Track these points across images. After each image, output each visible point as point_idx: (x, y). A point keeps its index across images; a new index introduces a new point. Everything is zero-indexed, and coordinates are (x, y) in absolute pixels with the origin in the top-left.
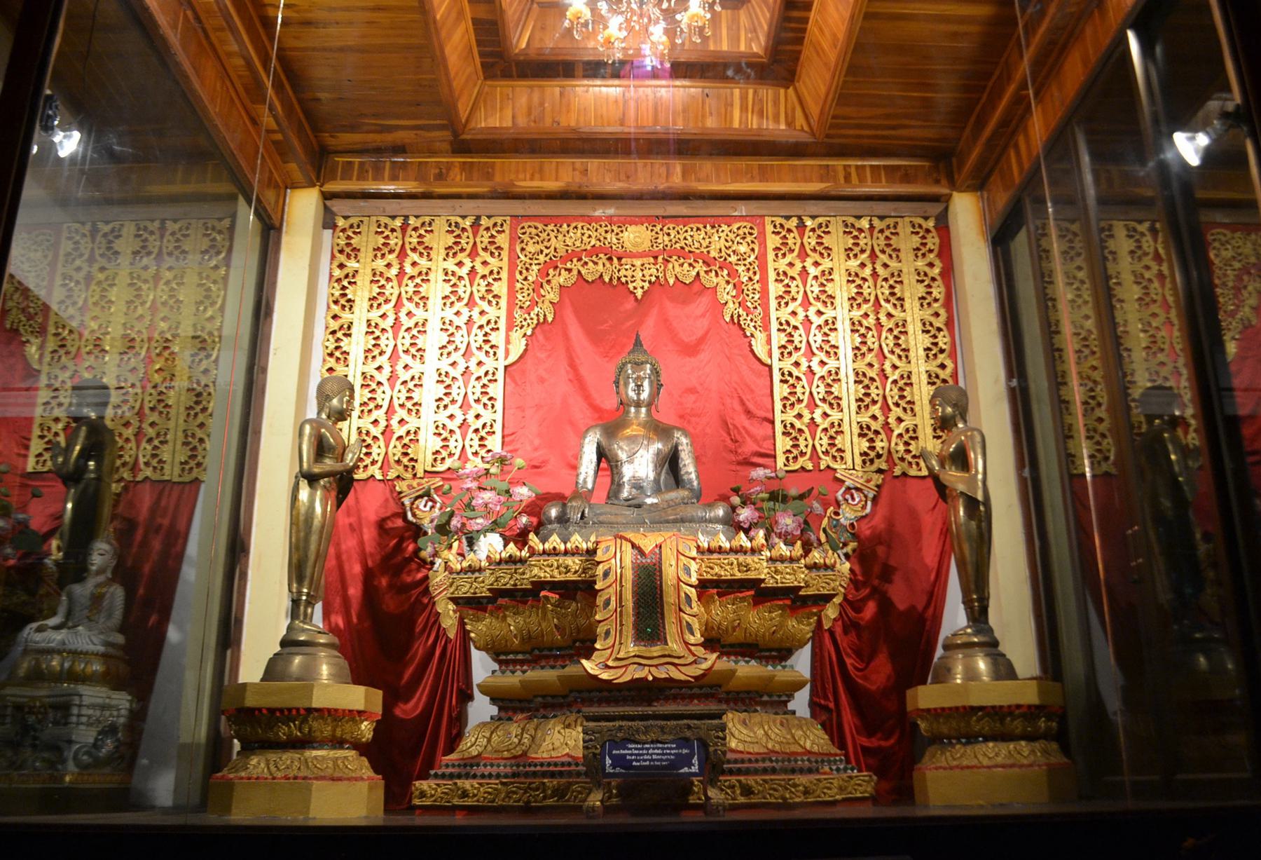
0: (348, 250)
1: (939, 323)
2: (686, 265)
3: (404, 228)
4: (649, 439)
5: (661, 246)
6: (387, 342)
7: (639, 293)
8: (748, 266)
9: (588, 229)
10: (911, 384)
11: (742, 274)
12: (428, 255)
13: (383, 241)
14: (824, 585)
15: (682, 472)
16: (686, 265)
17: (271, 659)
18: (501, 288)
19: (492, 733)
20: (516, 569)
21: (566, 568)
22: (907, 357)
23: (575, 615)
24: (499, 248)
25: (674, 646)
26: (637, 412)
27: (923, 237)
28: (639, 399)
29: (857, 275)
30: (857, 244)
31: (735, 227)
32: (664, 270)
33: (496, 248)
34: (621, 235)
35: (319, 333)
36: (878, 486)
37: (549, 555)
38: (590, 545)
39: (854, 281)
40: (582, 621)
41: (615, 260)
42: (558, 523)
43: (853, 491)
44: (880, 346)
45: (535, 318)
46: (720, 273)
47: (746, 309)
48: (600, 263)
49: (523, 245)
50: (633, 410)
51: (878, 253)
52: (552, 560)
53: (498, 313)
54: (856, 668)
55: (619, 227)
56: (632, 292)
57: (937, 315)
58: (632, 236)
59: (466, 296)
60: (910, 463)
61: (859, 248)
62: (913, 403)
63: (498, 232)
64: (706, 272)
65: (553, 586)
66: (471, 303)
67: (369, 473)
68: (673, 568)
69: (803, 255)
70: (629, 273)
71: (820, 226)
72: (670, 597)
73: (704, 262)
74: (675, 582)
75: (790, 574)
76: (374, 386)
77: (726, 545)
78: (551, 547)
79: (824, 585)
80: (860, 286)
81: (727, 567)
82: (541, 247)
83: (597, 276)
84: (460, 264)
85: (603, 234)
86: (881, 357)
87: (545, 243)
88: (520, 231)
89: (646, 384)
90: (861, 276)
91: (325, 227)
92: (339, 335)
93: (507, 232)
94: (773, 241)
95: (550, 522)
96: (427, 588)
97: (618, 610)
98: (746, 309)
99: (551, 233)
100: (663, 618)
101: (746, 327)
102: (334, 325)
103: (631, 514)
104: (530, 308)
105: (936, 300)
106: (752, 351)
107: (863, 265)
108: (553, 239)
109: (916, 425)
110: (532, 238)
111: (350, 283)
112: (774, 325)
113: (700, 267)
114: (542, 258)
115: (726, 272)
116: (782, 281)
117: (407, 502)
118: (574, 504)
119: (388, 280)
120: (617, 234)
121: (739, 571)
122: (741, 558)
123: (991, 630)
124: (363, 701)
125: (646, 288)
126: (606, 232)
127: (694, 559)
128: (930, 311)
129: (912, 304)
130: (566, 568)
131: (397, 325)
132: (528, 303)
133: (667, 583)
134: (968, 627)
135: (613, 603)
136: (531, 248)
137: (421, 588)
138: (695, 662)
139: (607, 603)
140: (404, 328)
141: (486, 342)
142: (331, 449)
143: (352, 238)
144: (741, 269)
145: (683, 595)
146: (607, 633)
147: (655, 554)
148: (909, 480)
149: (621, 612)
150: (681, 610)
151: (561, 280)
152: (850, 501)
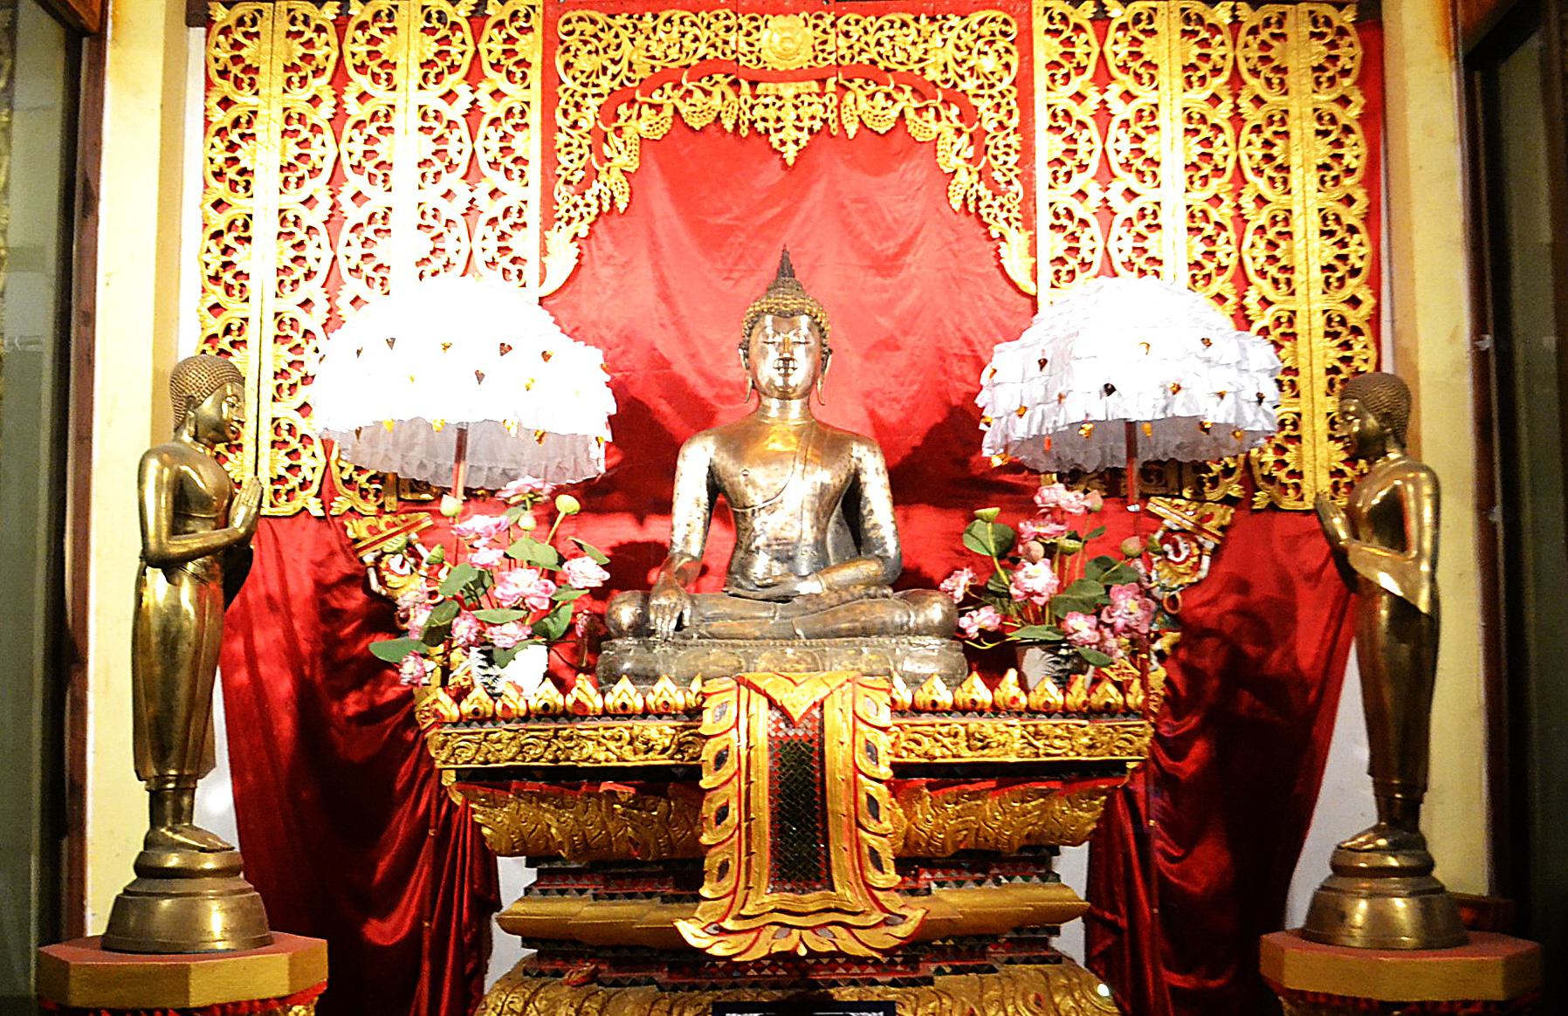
0: (235, 70)
1: (1352, 216)
2: (880, 97)
3: (341, 23)
4: (806, 461)
5: (832, 59)
6: (317, 253)
7: (790, 153)
8: (998, 99)
9: (693, 24)
10: (1294, 335)
11: (986, 115)
12: (389, 79)
13: (302, 50)
14: (1122, 744)
15: (867, 525)
16: (880, 97)
17: (118, 898)
18: (528, 144)
19: (527, 1004)
20: (557, 731)
21: (646, 743)
22: (1289, 282)
23: (665, 821)
24: (521, 63)
25: (846, 893)
26: (784, 408)
27: (1333, 45)
28: (786, 385)
29: (1203, 119)
30: (1205, 57)
31: (975, 18)
32: (838, 107)
33: (517, 64)
34: (756, 35)
35: (193, 241)
36: (1222, 528)
37: (614, 717)
38: (692, 700)
39: (1197, 132)
40: (677, 833)
41: (745, 86)
42: (636, 636)
43: (1178, 537)
44: (1241, 260)
45: (595, 203)
46: (943, 113)
47: (993, 185)
48: (716, 91)
49: (569, 57)
50: (774, 404)
51: (1246, 76)
52: (620, 726)
53: (525, 192)
54: (1171, 859)
55: (753, 19)
56: (776, 151)
57: (1349, 200)
58: (777, 38)
59: (463, 161)
60: (1285, 486)
61: (1209, 66)
62: (1296, 372)
63: (520, 30)
64: (918, 111)
65: (621, 774)
66: (472, 174)
67: (296, 505)
68: (847, 747)
69: (1103, 78)
70: (772, 113)
71: (1137, 19)
72: (839, 804)
73: (914, 91)
74: (850, 774)
75: (1062, 738)
76: (297, 338)
77: (945, 698)
78: (618, 704)
79: (1122, 744)
80: (1207, 142)
81: (947, 741)
82: (603, 60)
83: (711, 119)
84: (450, 96)
85: (722, 33)
86: (1242, 282)
87: (611, 54)
88: (562, 29)
89: (799, 352)
90: (1211, 121)
91: (190, 23)
92: (228, 239)
93: (539, 30)
94: (1046, 49)
95: (621, 634)
96: (412, 714)
97: (744, 825)
98: (993, 185)
99: (622, 31)
100: (826, 840)
101: (989, 220)
102: (220, 221)
103: (771, 616)
104: (585, 184)
105: (1350, 172)
106: (1001, 267)
107: (1215, 100)
108: (626, 45)
109: (1299, 415)
110: (585, 43)
111: (242, 136)
112: (1044, 218)
113: (907, 100)
114: (605, 83)
115: (955, 110)
116: (1061, 129)
117: (369, 558)
118: (663, 601)
119: (315, 129)
120: (749, 34)
121: (969, 747)
122: (974, 723)
123: (1421, 843)
124: (286, 982)
125: (803, 143)
126: (728, 29)
127: (885, 729)
128: (1338, 193)
129: (1304, 179)
130: (646, 743)
131: (334, 217)
132: (580, 174)
133: (834, 779)
134: (1378, 831)
135: (733, 815)
136: (585, 63)
137: (400, 716)
138: (885, 922)
139: (722, 814)
140: (348, 225)
141: (503, 250)
142: (204, 502)
143: (242, 46)
144: (983, 104)
145: (863, 798)
146: (724, 868)
147: (812, 720)
148: (1278, 516)
149: (748, 828)
150: (859, 825)
151: (642, 127)
152: (1171, 556)
